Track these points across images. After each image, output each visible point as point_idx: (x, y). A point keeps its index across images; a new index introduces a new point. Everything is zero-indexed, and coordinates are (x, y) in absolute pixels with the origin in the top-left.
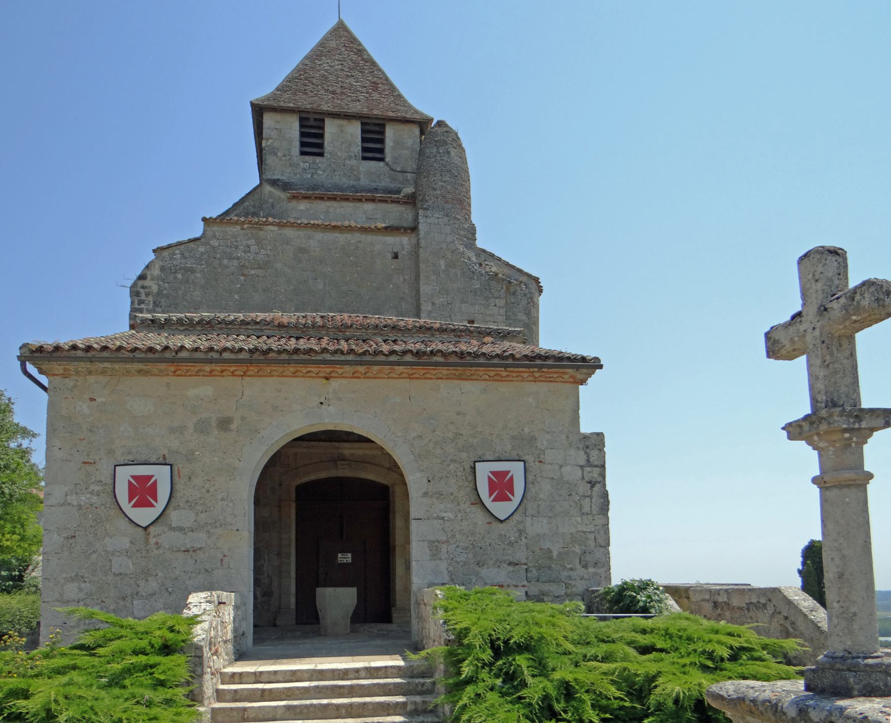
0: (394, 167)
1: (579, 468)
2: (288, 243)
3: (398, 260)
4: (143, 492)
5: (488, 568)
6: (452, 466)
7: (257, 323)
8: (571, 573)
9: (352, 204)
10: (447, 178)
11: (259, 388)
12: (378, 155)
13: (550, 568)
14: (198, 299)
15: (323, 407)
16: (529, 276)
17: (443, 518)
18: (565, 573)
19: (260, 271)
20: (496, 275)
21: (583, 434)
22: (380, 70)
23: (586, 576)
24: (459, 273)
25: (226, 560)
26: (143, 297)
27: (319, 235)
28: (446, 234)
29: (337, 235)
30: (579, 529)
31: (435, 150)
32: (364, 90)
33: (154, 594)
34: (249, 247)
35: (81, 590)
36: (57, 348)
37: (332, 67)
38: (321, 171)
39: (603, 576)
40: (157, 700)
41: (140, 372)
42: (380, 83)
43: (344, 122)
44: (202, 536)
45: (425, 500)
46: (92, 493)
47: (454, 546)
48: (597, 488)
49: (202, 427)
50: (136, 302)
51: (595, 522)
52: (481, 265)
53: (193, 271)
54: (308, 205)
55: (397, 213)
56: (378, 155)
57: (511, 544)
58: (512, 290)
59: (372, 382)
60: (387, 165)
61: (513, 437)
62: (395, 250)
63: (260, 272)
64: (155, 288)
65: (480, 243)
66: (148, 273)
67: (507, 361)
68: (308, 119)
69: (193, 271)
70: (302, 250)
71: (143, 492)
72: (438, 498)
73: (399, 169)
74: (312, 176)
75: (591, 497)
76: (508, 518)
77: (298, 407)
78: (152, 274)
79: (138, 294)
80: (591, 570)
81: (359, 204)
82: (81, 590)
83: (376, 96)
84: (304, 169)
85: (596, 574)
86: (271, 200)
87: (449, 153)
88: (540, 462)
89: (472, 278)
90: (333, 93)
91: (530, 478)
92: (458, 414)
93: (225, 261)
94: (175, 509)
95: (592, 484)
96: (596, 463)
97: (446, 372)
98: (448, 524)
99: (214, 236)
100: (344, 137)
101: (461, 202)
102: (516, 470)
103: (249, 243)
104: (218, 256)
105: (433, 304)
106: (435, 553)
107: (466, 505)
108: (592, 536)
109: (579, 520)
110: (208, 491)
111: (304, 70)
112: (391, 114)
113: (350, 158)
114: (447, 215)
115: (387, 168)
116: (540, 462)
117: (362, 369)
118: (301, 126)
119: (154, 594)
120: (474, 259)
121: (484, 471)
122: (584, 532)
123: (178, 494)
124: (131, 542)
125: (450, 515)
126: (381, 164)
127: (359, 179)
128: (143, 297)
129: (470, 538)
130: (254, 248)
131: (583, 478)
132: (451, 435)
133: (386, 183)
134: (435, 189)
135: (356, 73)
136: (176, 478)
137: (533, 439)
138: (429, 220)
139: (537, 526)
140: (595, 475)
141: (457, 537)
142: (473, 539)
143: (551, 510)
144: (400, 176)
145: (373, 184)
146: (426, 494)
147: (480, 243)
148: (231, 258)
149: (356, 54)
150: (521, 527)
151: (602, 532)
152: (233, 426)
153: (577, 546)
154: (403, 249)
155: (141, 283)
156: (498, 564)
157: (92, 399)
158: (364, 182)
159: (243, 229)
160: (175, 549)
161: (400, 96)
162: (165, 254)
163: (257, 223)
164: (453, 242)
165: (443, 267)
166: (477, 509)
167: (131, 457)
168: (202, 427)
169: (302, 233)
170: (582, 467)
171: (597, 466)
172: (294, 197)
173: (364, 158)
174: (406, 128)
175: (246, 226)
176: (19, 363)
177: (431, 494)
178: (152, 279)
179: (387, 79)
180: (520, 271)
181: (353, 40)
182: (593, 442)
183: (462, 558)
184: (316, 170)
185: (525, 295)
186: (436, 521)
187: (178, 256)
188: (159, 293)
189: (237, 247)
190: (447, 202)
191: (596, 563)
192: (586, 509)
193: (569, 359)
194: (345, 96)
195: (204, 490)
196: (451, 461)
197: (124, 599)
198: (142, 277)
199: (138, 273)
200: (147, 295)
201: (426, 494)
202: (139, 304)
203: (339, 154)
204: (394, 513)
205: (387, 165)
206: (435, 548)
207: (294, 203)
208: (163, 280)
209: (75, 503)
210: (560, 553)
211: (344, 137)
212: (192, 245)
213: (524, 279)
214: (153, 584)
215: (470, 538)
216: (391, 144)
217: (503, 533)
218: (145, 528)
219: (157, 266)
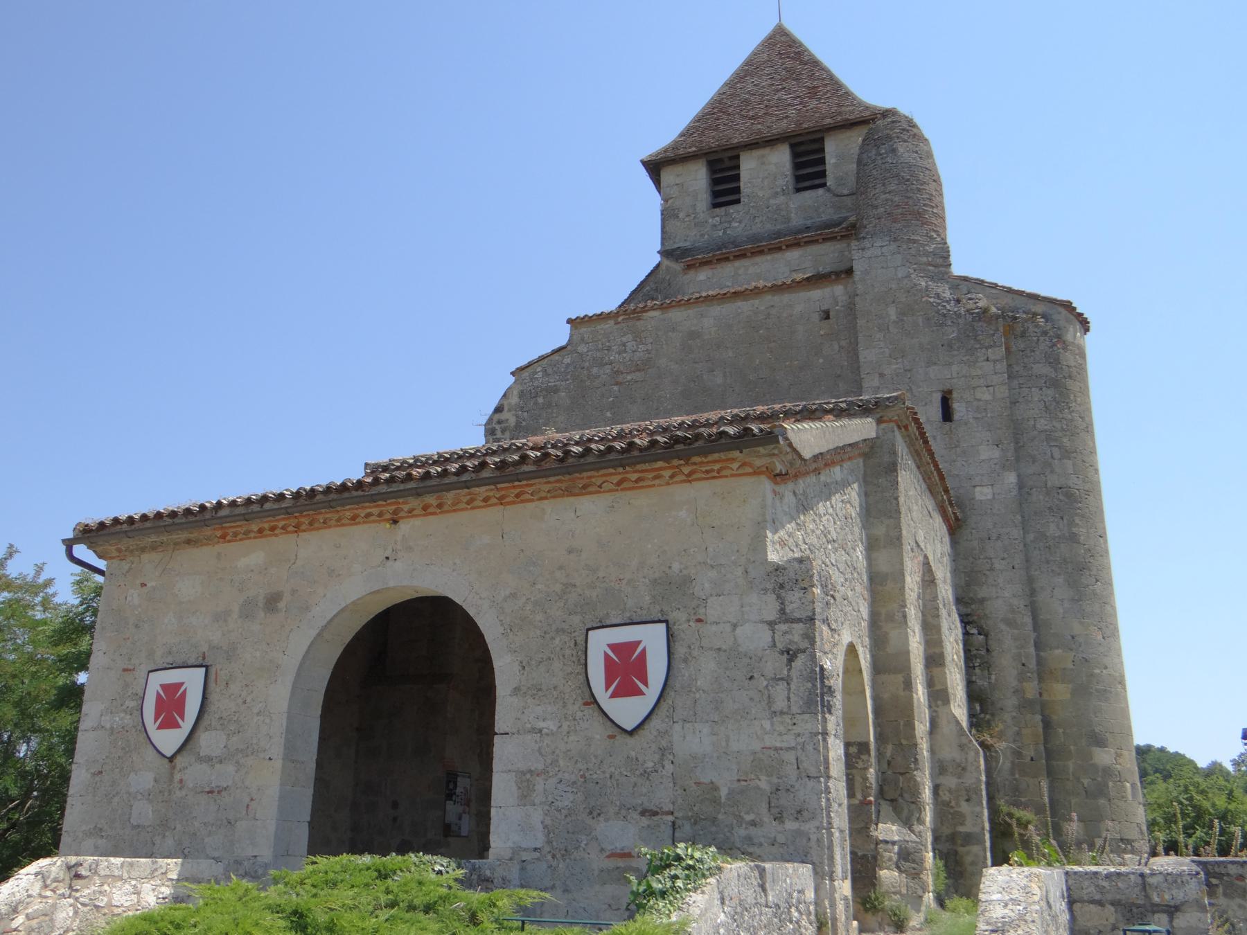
1: (766, 627)
2: (674, 330)
3: (831, 321)
5: (607, 820)
6: (557, 641)
8: (753, 831)
9: (769, 257)
10: (892, 187)
12: (817, 182)
13: (714, 821)
15: (390, 563)
17: (540, 731)
18: (742, 832)
19: (638, 374)
20: (986, 310)
21: (773, 563)
23: (781, 839)
24: (920, 320)
25: (253, 805)
27: (716, 310)
28: (896, 268)
29: (739, 304)
30: (768, 744)
31: (874, 152)
32: (797, 101)
34: (624, 345)
36: (102, 525)
38: (739, 222)
39: (813, 837)
41: (188, 542)
43: (766, 151)
45: (515, 700)
47: (555, 780)
48: (799, 663)
49: (247, 612)
51: (797, 729)
52: (958, 301)
53: (556, 390)
55: (825, 255)
57: (646, 774)
58: (1019, 329)
59: (452, 518)
61: (655, 582)
62: (825, 307)
63: (638, 376)
66: (505, 403)
68: (720, 160)
69: (556, 390)
70: (693, 335)
72: (533, 696)
73: (846, 192)
75: (788, 680)
76: (640, 726)
78: (509, 404)
80: (790, 825)
81: (778, 255)
85: (799, 833)
87: (894, 151)
88: (699, 620)
89: (942, 325)
91: (680, 650)
93: (595, 370)
94: (206, 729)
95: (791, 655)
96: (797, 615)
97: (546, 487)
98: (547, 741)
99: (583, 340)
100: (765, 172)
101: (919, 215)
102: (652, 639)
103: (624, 339)
105: (882, 375)
106: (525, 797)
107: (576, 707)
108: (790, 757)
109: (767, 725)
110: (245, 702)
112: (829, 121)
113: (776, 195)
114: (895, 240)
116: (699, 620)
117: (431, 500)
121: (600, 642)
122: (776, 749)
123: (212, 708)
124: (156, 781)
125: (550, 725)
126: (821, 191)
129: (580, 765)
131: (774, 645)
132: (558, 588)
133: (828, 214)
134: (876, 207)
135: (791, 84)
136: (212, 685)
137: (687, 581)
138: (868, 253)
139: (693, 741)
140: (797, 638)
141: (561, 763)
142: (584, 767)
143: (717, 708)
146: (516, 691)
149: (793, 59)
150: (664, 743)
151: (810, 748)
152: (281, 605)
153: (763, 778)
155: (497, 417)
156: (624, 812)
157: (143, 585)
158: (796, 221)
160: (199, 790)
162: (526, 374)
163: (634, 312)
164: (908, 276)
166: (590, 711)
167: (170, 659)
168: (247, 612)
169: (691, 312)
170: (771, 624)
171: (799, 620)
172: (689, 267)
173: (798, 190)
175: (620, 319)
176: (64, 547)
177: (524, 689)
178: (509, 410)
182: (792, 575)
183: (566, 802)
184: (730, 222)
185: (1045, 333)
186: (529, 737)
191: (799, 812)
192: (780, 704)
195: (240, 701)
196: (558, 631)
198: (498, 410)
200: (503, 431)
203: (760, 194)
206: (526, 781)
208: (522, 409)
209: (108, 726)
210: (731, 792)
211: (765, 172)
212: (556, 357)
213: (1039, 308)
215: (580, 765)
217: (633, 754)
219: (515, 392)
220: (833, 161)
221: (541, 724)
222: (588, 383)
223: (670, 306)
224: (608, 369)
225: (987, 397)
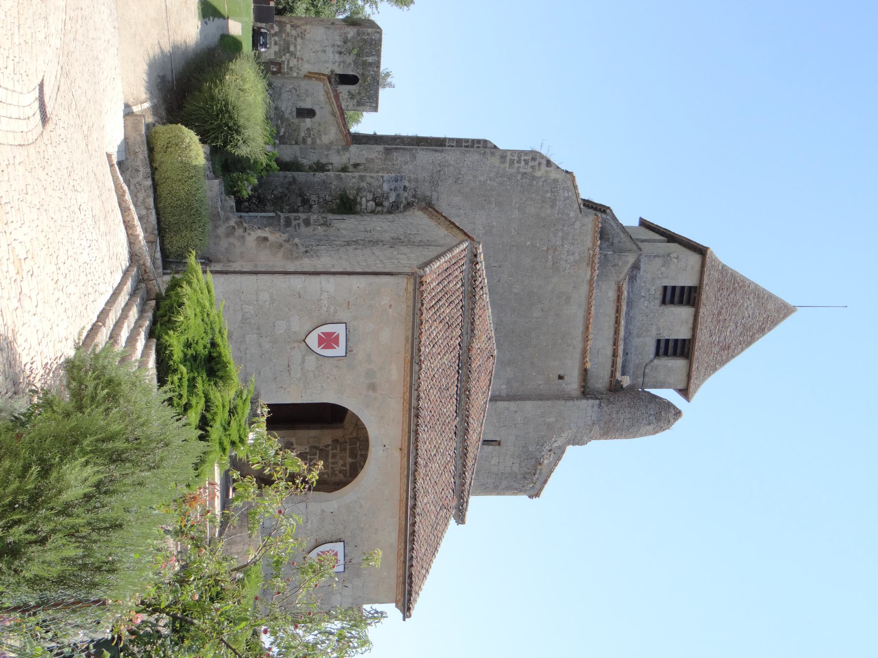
0: (649, 367)
4: (328, 340)
7: (472, 331)
10: (626, 422)
11: (395, 408)
12: (662, 351)
14: (527, 211)
15: (382, 447)
16: (541, 490)
22: (742, 350)
26: (531, 164)
27: (581, 314)
31: (652, 412)
32: (722, 338)
33: (260, 346)
35: (265, 302)
37: (747, 309)
42: (727, 351)
43: (690, 325)
44: (299, 375)
46: (329, 307)
50: (526, 158)
52: (550, 450)
53: (552, 207)
56: (662, 351)
58: (528, 476)
60: (651, 361)
63: (550, 264)
65: (570, 449)
67: (461, 475)
69: (552, 207)
70: (568, 299)
71: (328, 340)
73: (647, 371)
74: (643, 297)
77: (383, 429)
79: (534, 159)
81: (611, 342)
82: (265, 302)
83: (716, 349)
86: (620, 263)
87: (649, 424)
90: (720, 313)
92: (376, 530)
93: (560, 234)
99: (584, 225)
100: (676, 322)
103: (576, 254)
104: (565, 228)
105: (516, 412)
111: (744, 286)
114: (594, 424)
115: (648, 361)
118: (690, 288)
119: (260, 346)
120: (555, 444)
126: (652, 356)
127: (638, 337)
128: (531, 164)
130: (571, 258)
133: (634, 359)
134: (617, 413)
138: (589, 409)
144: (641, 372)
145: (633, 349)
146: (323, 511)
147: (570, 449)
148: (563, 239)
152: (371, 393)
154: (567, 384)
155: (544, 162)
158: (636, 341)
159: (589, 249)
161: (715, 369)
163: (593, 262)
165: (548, 420)
166: (313, 543)
173: (659, 341)
174: (684, 377)
175: (591, 252)
178: (546, 171)
179: (733, 357)
180: (545, 482)
181: (775, 323)
187: (566, 194)
188: (534, 178)
189: (573, 244)
190: (605, 423)
193: (410, 594)
194: (715, 323)
197: (258, 328)
198: (549, 163)
199: (552, 159)
200: (533, 167)
201: (323, 511)
202: (525, 160)
203: (662, 320)
204: (321, 428)
205: (651, 361)
207: (614, 287)
208: (545, 181)
211: (676, 322)
213: (538, 486)
214: (267, 346)
218: (304, 341)
220: (670, 365)
221: (310, 522)
222: (553, 229)
223: (591, 285)
224: (559, 243)
225: (493, 462)
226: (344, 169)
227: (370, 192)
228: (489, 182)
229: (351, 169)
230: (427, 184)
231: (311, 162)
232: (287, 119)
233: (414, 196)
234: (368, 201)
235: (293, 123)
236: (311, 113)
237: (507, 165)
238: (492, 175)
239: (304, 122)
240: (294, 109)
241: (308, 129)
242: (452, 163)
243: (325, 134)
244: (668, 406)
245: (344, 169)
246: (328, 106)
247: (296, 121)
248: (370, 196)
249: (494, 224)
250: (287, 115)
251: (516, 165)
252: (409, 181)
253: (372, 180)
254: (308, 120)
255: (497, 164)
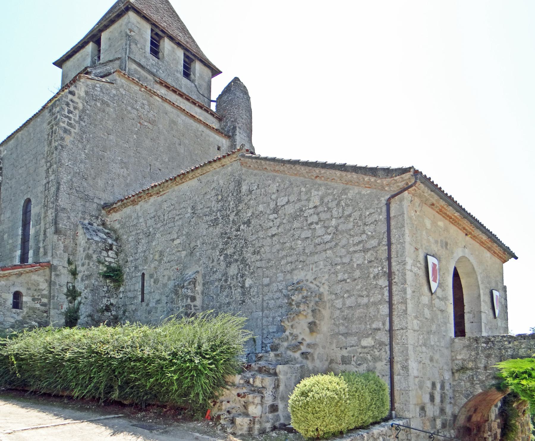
40: (315, 225)
53: (108, 105)
54: (166, 92)
63: (150, 126)
64: (80, 106)
81: (193, 106)
84: (152, 64)
93: (129, 108)
104: (125, 102)
128: (72, 109)
159: (140, 90)
169: (175, 111)
187: (99, 89)
188: (84, 111)
189: (136, 101)
200: (75, 108)
216: (198, 75)
226: (74, 273)
227: (101, 252)
228: (86, 151)
229: (73, 267)
230: (87, 204)
231: (66, 300)
232: (24, 318)
233: (97, 218)
234: (108, 256)
235: (27, 313)
236: (17, 295)
237: (72, 130)
238: (80, 146)
239: (26, 302)
240: (14, 310)
241: (34, 300)
242: (69, 177)
243: (38, 285)
244: (228, 90)
245: (74, 273)
246: (11, 278)
247: (25, 310)
248: (104, 253)
249: (119, 158)
250: (20, 318)
251: (72, 122)
252: (85, 219)
253: (91, 248)
254: (25, 299)
255: (72, 139)
